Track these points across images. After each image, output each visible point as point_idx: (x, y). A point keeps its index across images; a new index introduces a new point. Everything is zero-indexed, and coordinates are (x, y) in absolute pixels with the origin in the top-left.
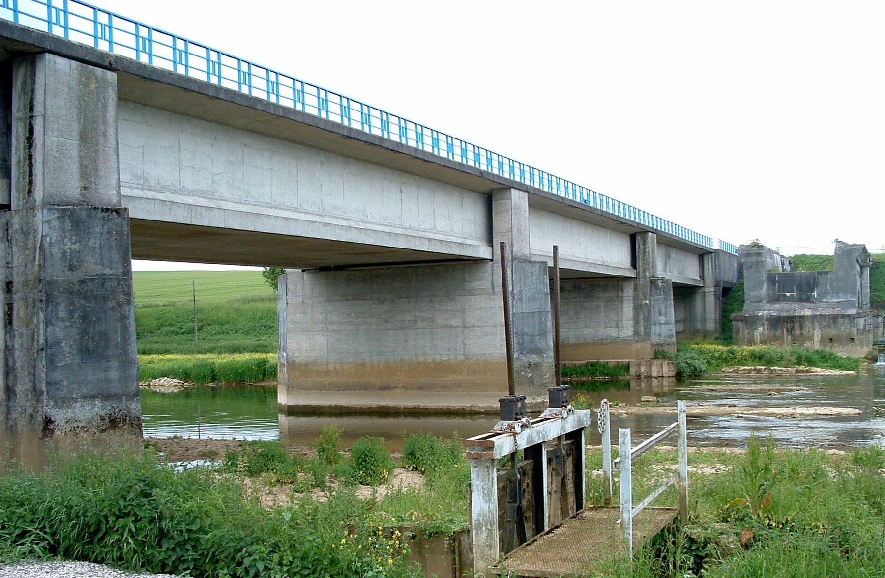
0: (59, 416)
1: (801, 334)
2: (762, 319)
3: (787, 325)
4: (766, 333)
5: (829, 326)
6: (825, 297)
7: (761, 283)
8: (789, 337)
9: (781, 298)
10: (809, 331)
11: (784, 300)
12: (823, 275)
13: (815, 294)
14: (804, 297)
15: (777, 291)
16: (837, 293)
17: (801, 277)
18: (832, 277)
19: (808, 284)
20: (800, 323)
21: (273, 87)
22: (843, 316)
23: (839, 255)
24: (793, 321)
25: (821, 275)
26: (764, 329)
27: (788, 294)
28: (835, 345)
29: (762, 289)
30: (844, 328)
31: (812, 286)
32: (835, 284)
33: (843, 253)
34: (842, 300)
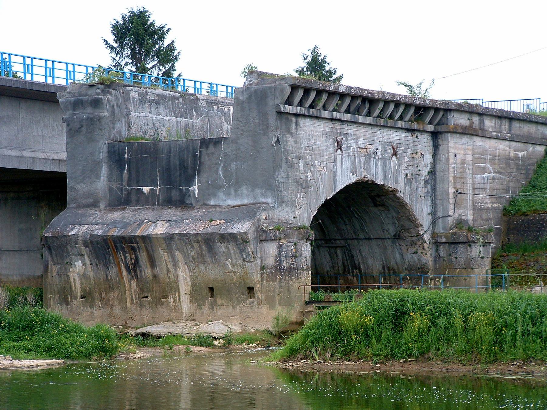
0: (492, 234)
1: (155, 276)
2: (76, 243)
3: (125, 258)
4: (90, 272)
5: (201, 258)
6: (214, 195)
7: (97, 164)
8: (134, 284)
9: (134, 197)
10: (168, 271)
11: (138, 202)
12: (211, 148)
13: (195, 188)
14: (175, 194)
15: (125, 183)
16: (237, 185)
17: (170, 152)
18: (227, 151)
19: (183, 166)
20: (148, 251)
21: (50, 71)
22: (223, 238)
23: (242, 103)
24: (133, 249)
25: (207, 147)
26: (84, 264)
27: (146, 190)
28: (219, 301)
29: (98, 177)
30: (232, 264)
31: (190, 171)
32: (233, 166)
33: (250, 96)
34: (246, 201)
